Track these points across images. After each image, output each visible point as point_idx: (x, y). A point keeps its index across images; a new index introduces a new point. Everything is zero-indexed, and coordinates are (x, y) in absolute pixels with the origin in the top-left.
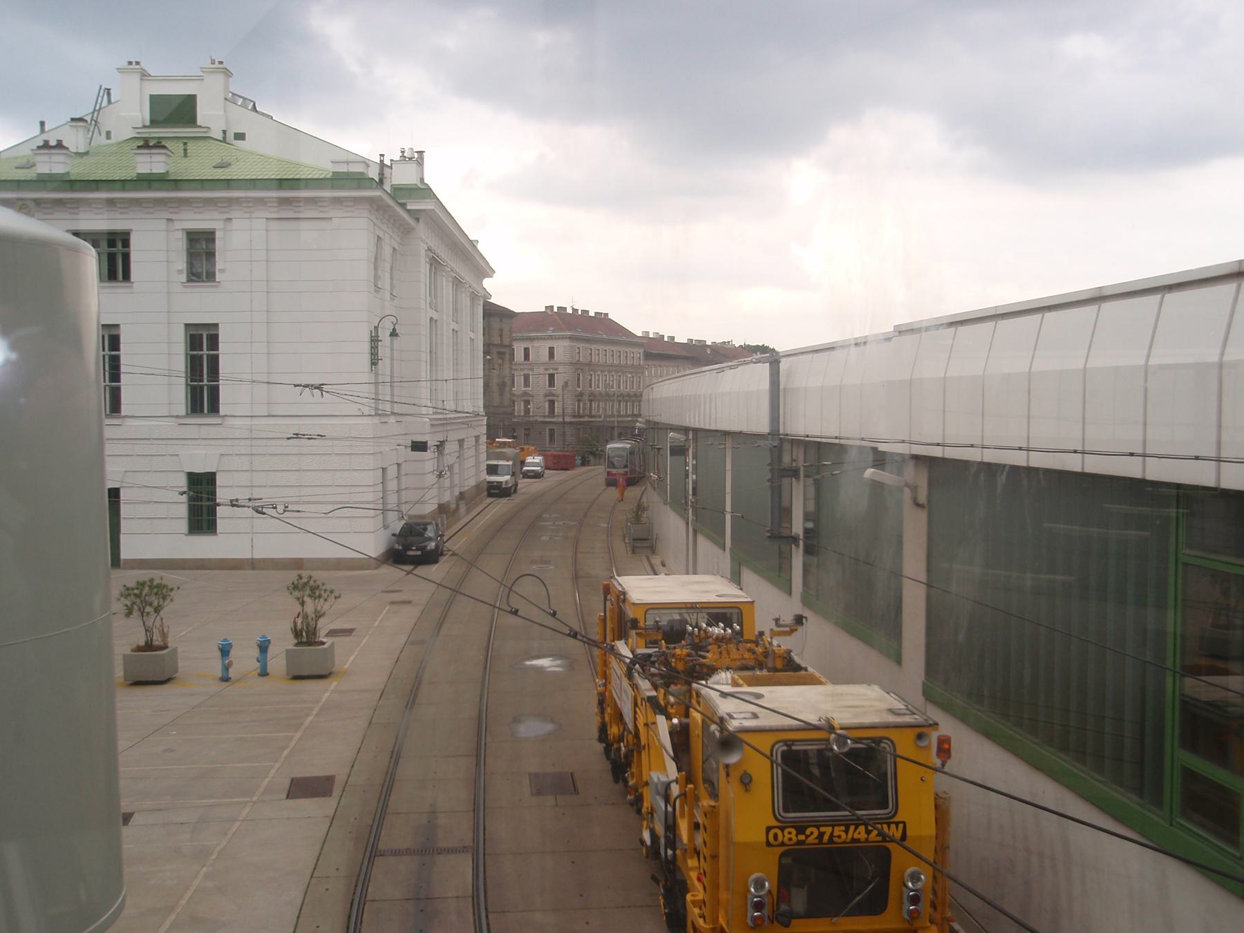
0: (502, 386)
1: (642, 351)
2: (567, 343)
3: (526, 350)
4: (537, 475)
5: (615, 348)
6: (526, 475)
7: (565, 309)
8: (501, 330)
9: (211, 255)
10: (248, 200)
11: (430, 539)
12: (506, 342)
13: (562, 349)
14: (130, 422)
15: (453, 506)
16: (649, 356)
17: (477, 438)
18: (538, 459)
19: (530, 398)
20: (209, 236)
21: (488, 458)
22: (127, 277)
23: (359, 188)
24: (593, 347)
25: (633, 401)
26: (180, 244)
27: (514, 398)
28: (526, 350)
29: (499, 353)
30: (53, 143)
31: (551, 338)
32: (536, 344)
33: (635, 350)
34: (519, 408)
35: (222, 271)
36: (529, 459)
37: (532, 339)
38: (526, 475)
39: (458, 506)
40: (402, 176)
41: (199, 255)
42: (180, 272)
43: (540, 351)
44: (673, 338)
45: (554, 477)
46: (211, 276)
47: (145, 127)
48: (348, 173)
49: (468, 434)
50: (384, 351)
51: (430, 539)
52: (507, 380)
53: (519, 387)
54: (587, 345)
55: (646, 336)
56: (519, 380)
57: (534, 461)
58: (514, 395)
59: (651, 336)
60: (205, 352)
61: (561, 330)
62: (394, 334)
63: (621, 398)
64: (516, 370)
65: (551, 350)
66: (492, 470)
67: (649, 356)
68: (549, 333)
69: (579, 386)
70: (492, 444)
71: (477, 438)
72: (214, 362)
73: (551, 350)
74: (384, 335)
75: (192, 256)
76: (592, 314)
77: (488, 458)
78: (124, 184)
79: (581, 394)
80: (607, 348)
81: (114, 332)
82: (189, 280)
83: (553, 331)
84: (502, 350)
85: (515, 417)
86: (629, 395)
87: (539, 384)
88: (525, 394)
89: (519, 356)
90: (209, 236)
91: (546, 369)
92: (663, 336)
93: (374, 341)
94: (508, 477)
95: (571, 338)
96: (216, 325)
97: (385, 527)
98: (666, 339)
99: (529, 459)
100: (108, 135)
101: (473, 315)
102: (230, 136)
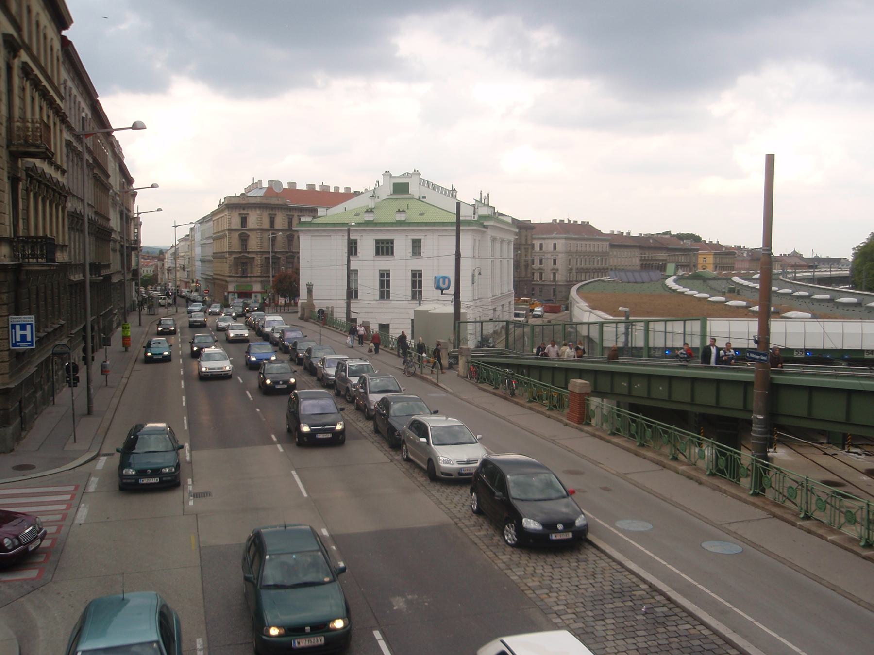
0: (527, 266)
1: (608, 243)
2: (563, 241)
3: (541, 245)
4: (539, 316)
5: (592, 243)
6: (535, 316)
7: (563, 221)
8: (526, 236)
9: (420, 247)
10: (432, 230)
11: (490, 343)
12: (529, 242)
13: (561, 244)
14: (393, 302)
15: (499, 331)
16: (612, 246)
17: (510, 302)
18: (540, 309)
19: (543, 271)
20: (419, 241)
21: (515, 310)
22: (392, 254)
23: (469, 226)
24: (578, 242)
25: (602, 273)
26: (410, 243)
27: (534, 271)
28: (541, 245)
29: (525, 249)
30: (401, 210)
31: (555, 238)
32: (547, 241)
33: (604, 243)
34: (537, 276)
35: (423, 253)
36: (536, 309)
37: (544, 239)
38: (535, 316)
39: (501, 332)
40: (483, 211)
41: (416, 247)
42: (410, 253)
43: (548, 245)
44: (629, 234)
45: (549, 316)
46: (420, 254)
47: (391, 194)
48: (465, 220)
49: (506, 302)
50: (476, 278)
51: (490, 343)
52: (530, 262)
53: (537, 265)
54: (575, 242)
55: (612, 235)
56: (537, 262)
57: (538, 310)
58: (534, 269)
59: (615, 233)
60: (417, 279)
61: (560, 233)
62: (480, 274)
63: (594, 271)
64: (535, 255)
65: (555, 245)
66: (517, 315)
67: (612, 246)
68: (553, 236)
69: (570, 265)
70: (519, 300)
71: (510, 302)
72: (420, 282)
73: (555, 245)
74: (476, 273)
75: (414, 247)
76: (579, 222)
77: (515, 310)
78: (392, 224)
79: (571, 269)
80: (587, 243)
81: (388, 272)
82: (412, 255)
83: (557, 234)
84: (527, 247)
85: (534, 281)
86: (599, 269)
87: (548, 264)
88: (540, 269)
89: (537, 248)
90: (419, 241)
91: (552, 255)
92: (623, 233)
93: (473, 276)
94: (523, 319)
95: (566, 239)
96: (421, 270)
97: (476, 338)
98: (625, 234)
99: (536, 309)
100: (378, 197)
101: (508, 252)
102: (421, 197)
